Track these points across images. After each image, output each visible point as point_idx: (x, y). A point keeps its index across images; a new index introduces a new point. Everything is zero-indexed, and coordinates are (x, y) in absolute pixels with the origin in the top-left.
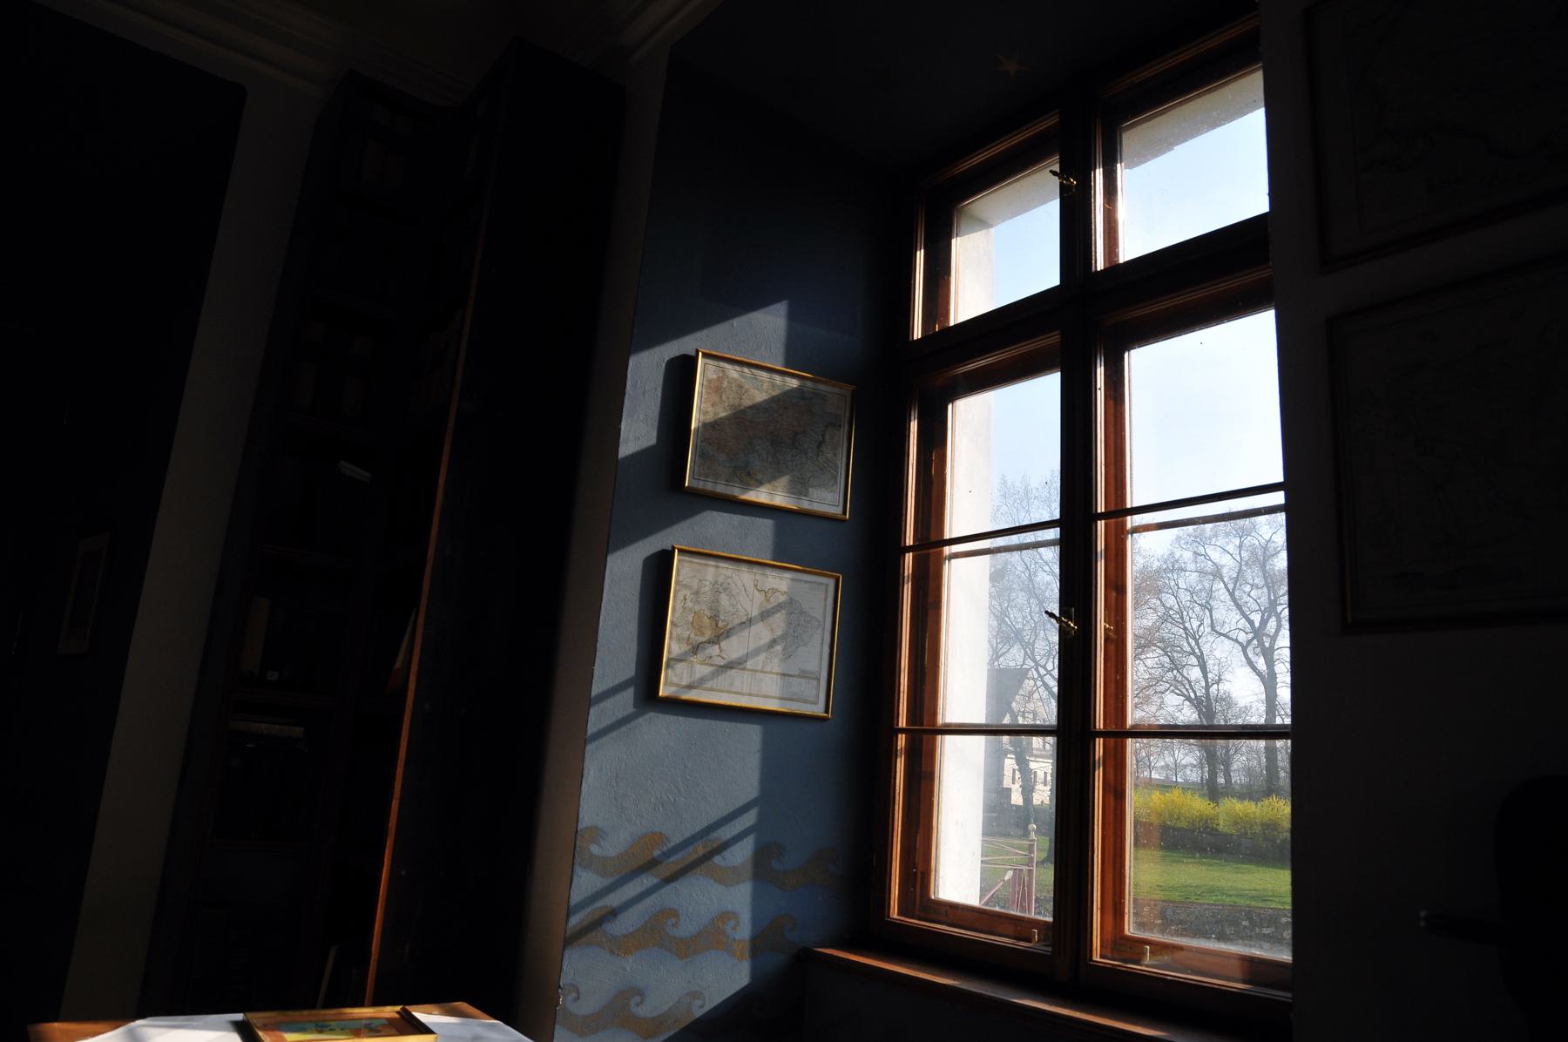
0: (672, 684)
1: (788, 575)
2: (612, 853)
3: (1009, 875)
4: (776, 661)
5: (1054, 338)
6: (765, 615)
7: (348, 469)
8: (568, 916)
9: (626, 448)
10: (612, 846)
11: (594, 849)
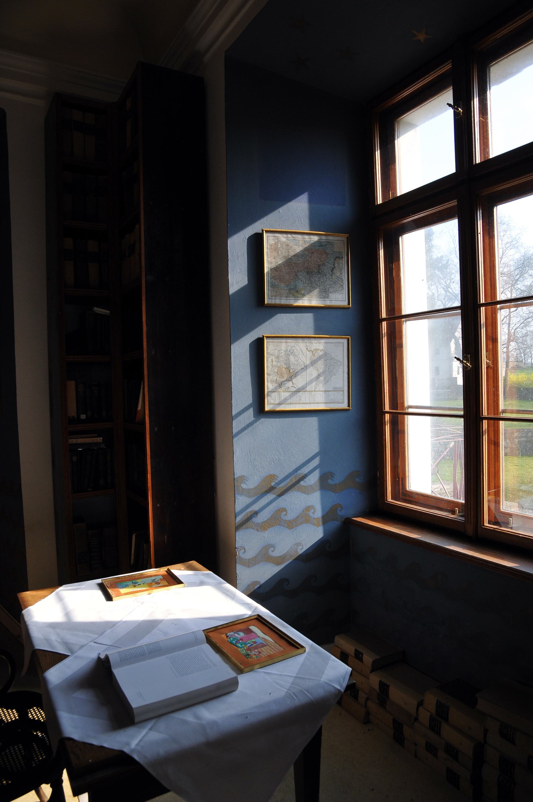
0: (271, 404)
1: (323, 341)
2: (252, 486)
3: (452, 444)
4: (321, 385)
5: (454, 203)
6: (313, 363)
7: (98, 310)
8: (236, 517)
9: (232, 290)
10: (252, 483)
11: (244, 486)
